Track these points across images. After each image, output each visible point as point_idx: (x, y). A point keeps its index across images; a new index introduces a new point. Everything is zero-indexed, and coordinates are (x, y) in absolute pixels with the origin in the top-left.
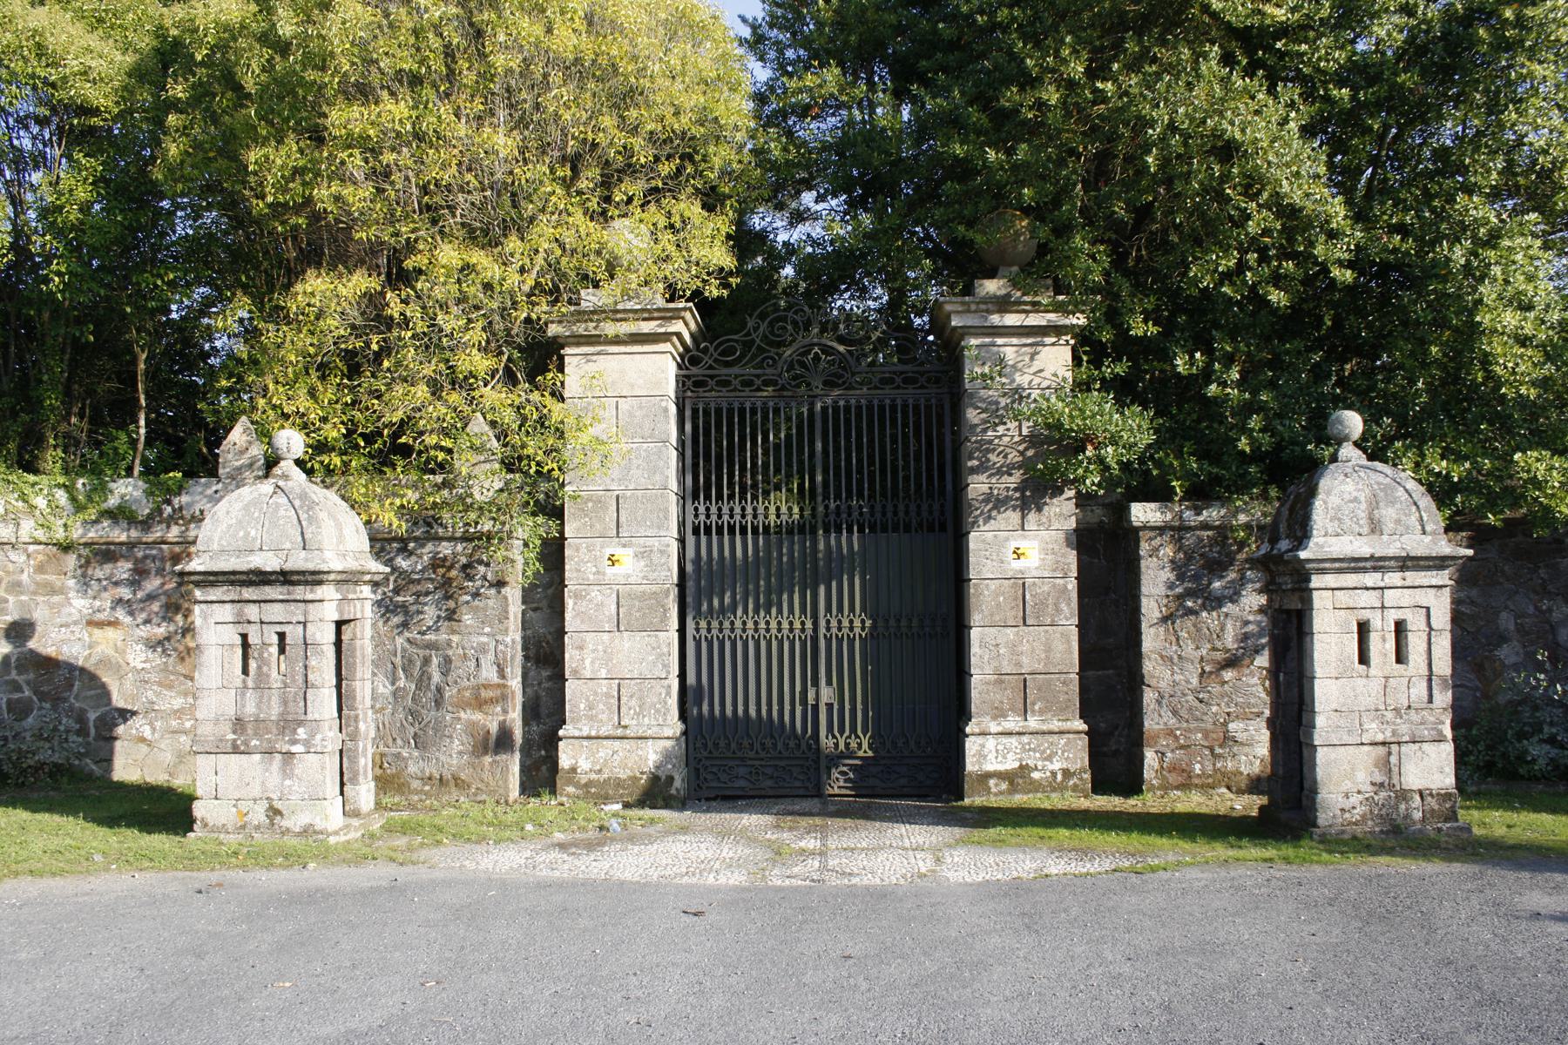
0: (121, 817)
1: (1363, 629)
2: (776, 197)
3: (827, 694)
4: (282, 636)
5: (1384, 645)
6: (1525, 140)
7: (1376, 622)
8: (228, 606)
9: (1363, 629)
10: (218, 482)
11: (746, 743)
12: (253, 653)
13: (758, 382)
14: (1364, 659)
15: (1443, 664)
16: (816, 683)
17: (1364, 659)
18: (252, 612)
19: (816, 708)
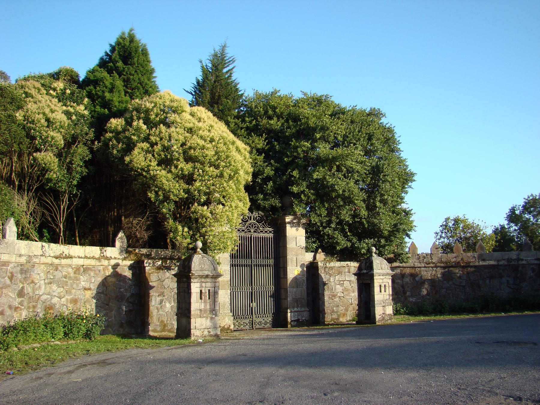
0: (361, 299)
1: (380, 286)
2: (35, 148)
3: (254, 304)
4: (209, 290)
5: (383, 289)
6: (144, 91)
7: (382, 285)
8: (199, 283)
9: (380, 286)
10: (464, 250)
11: (238, 317)
12: (203, 294)
13: (241, 230)
14: (381, 292)
15: (391, 293)
16: (252, 302)
17: (381, 292)
18: (204, 285)
19: (252, 308)
